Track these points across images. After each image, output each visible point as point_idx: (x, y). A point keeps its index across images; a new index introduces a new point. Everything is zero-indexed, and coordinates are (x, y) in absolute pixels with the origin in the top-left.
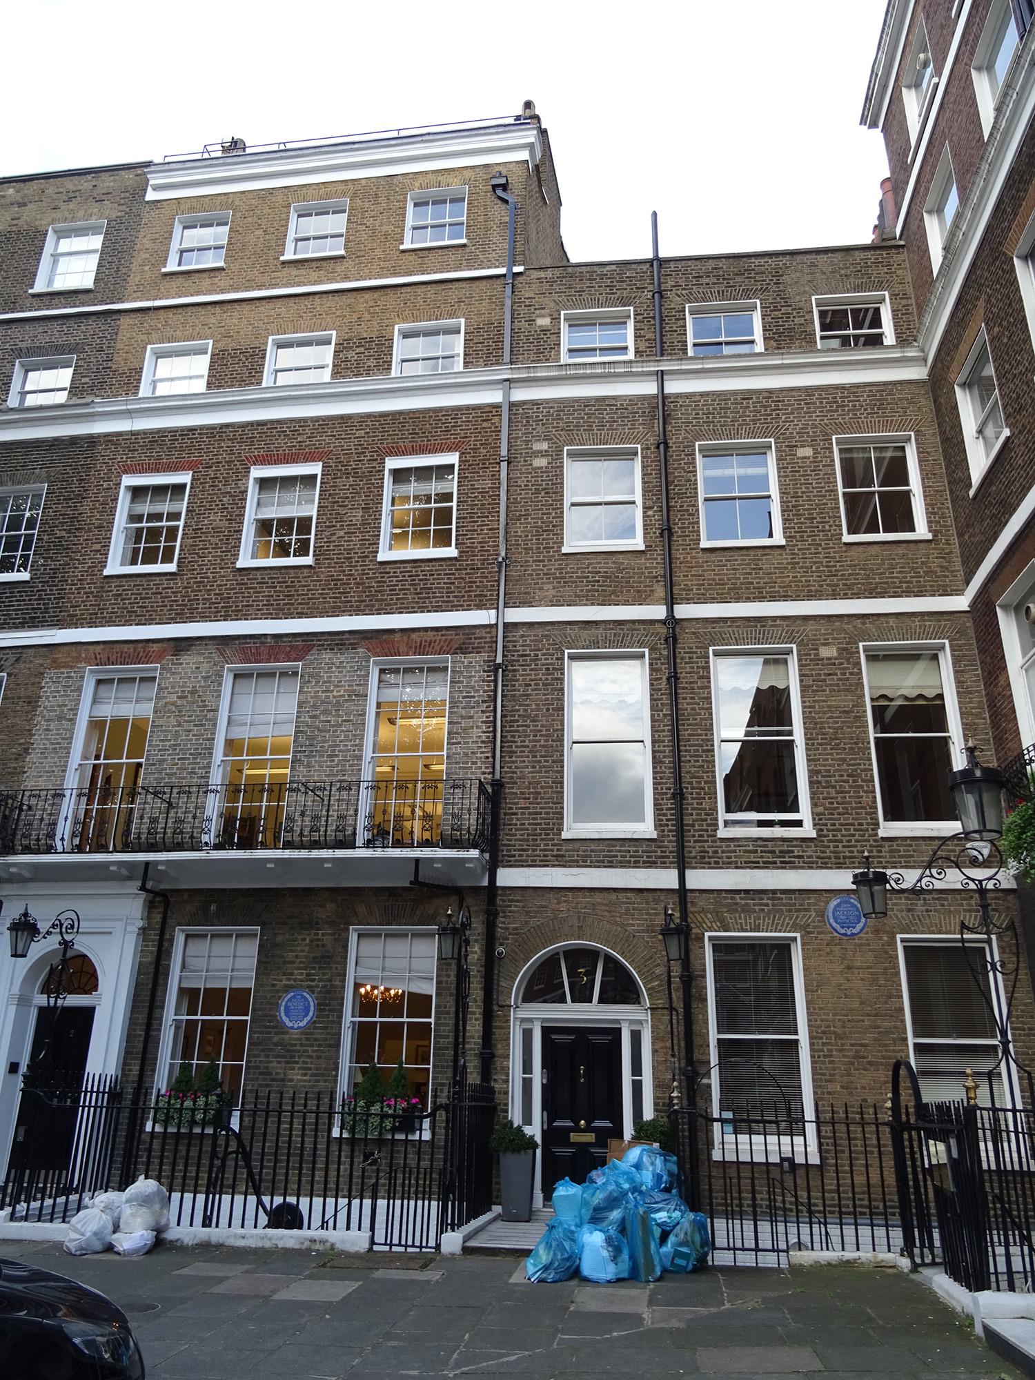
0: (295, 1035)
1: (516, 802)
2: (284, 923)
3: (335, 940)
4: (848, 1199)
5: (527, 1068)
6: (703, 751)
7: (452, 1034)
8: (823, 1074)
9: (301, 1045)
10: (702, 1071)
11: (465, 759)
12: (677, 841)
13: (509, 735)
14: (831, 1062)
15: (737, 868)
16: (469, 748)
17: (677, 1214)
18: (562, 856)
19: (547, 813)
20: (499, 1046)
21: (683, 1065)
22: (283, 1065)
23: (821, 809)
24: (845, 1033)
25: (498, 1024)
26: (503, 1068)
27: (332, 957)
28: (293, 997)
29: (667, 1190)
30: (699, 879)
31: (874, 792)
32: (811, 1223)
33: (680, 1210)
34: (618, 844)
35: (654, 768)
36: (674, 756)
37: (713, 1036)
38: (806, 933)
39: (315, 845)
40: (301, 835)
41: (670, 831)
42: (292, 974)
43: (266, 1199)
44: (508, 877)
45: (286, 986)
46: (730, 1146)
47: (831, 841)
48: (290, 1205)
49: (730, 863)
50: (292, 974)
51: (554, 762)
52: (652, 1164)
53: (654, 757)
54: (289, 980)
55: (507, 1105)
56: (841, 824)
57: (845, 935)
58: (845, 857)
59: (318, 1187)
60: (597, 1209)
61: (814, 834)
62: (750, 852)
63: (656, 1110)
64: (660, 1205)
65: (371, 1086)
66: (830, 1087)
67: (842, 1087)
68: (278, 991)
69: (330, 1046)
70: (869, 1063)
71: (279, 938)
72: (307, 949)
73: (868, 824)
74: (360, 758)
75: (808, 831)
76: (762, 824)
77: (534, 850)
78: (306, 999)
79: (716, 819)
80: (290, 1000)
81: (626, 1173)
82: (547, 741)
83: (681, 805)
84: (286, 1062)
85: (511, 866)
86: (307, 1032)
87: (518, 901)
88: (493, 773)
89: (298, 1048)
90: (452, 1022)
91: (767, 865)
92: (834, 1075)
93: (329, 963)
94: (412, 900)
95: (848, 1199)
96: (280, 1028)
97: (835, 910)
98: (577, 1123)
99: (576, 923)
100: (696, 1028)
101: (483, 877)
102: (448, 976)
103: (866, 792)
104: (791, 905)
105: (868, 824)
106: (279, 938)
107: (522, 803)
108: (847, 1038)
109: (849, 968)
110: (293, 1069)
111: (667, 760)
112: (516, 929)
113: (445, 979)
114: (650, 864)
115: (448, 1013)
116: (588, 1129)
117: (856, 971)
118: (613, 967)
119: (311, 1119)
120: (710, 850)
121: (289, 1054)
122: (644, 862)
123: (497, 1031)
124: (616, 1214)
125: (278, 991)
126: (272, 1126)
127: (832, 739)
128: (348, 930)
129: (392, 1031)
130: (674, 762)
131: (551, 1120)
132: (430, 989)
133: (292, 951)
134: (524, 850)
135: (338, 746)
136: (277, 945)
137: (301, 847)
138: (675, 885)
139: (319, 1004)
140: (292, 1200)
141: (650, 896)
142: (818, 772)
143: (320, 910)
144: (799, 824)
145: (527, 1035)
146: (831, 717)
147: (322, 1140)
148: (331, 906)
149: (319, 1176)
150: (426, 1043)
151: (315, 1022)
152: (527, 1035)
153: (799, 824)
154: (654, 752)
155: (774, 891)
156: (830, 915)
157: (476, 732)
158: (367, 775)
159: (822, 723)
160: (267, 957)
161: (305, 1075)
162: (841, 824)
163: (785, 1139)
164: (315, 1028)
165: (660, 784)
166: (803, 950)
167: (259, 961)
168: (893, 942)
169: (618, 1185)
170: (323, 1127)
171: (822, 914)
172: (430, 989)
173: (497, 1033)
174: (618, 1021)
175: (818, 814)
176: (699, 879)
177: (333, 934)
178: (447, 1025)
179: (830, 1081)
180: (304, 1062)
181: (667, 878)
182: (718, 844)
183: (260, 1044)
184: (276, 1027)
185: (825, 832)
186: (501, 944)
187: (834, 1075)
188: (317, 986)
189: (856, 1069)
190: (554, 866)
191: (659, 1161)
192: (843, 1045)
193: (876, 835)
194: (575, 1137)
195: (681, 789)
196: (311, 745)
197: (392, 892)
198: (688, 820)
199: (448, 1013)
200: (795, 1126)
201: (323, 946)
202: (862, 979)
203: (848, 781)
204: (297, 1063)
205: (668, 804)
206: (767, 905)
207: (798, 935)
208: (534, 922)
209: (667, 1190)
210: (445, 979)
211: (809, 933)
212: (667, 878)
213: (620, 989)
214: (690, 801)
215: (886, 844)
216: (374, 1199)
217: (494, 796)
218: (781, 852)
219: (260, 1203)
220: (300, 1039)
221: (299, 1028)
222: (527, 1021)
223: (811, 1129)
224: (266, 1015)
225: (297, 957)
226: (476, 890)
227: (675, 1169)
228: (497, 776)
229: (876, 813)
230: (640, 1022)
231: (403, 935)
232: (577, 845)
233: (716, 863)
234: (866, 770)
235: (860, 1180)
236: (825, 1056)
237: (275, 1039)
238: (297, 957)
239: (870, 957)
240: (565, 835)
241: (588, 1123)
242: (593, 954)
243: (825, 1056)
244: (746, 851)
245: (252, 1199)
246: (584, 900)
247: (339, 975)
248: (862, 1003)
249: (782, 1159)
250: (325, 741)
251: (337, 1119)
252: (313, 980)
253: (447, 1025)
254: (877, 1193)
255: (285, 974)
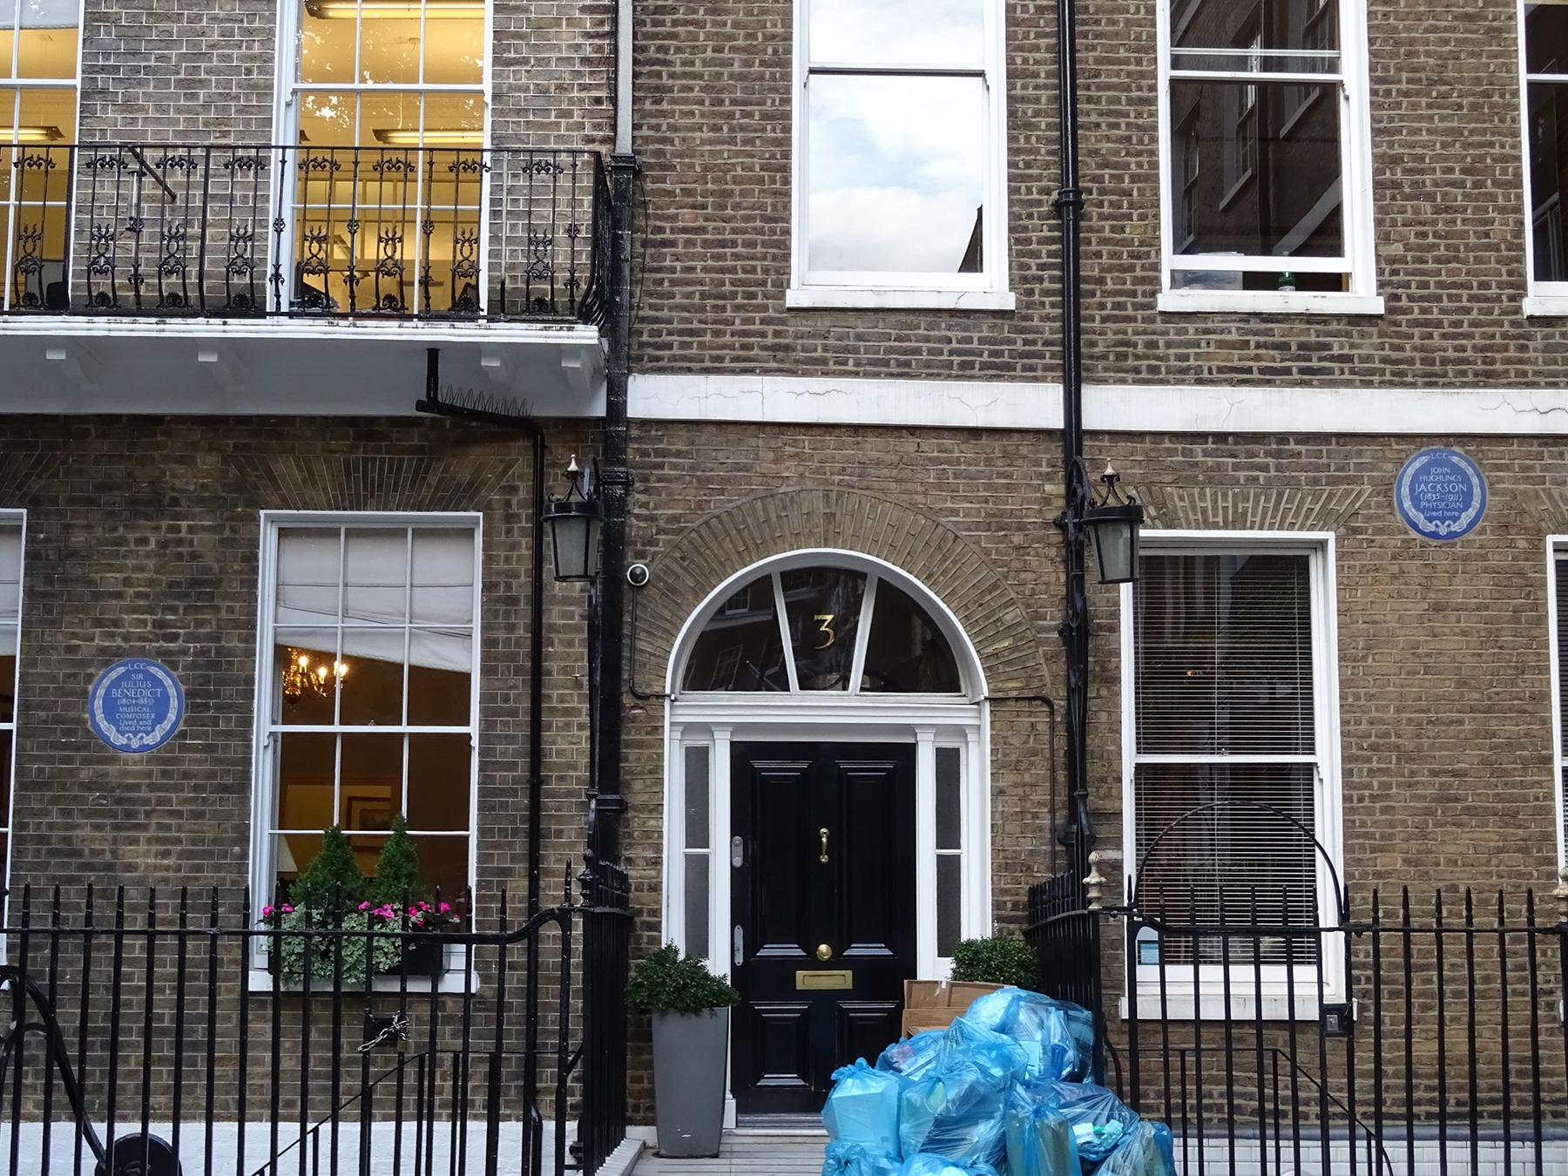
0: (135, 764)
1: (673, 210)
2: (89, 502)
3: (223, 542)
4: (1519, 1088)
5: (698, 832)
6: (1130, 101)
7: (523, 762)
8: (1367, 836)
9: (152, 787)
10: (1103, 832)
11: (540, 103)
12: (1063, 318)
13: (653, 44)
14: (1385, 810)
15: (1200, 382)
16: (550, 75)
17: (1115, 1126)
18: (787, 348)
19: (750, 244)
20: (638, 786)
21: (1059, 822)
22: (109, 833)
23: (1397, 249)
24: (1419, 748)
25: (633, 736)
26: (647, 834)
27: (217, 583)
28: (125, 677)
29: (1075, 1078)
30: (1112, 406)
31: (1519, 210)
32: (1353, 1139)
33: (1122, 1119)
34: (923, 321)
35: (1012, 139)
36: (1061, 113)
37: (1130, 758)
38: (1349, 532)
39: (173, 306)
40: (137, 279)
41: (1045, 293)
42: (116, 623)
43: (100, 1129)
44: (654, 396)
45: (103, 651)
46: (1170, 989)
47: (1416, 323)
48: (157, 1145)
49: (1185, 371)
50: (116, 623)
51: (765, 116)
52: (1041, 1025)
53: (1011, 114)
54: (112, 636)
55: (657, 913)
56: (1440, 285)
57: (1434, 535)
58: (1445, 361)
59: (226, 1098)
60: (942, 1123)
61: (1377, 306)
62: (1232, 345)
63: (997, 918)
64: (1078, 1110)
65: (324, 882)
66: (1382, 862)
67: (1406, 861)
68: (84, 663)
69: (224, 789)
70: (1467, 811)
71: (79, 539)
72: (151, 563)
73: (1500, 286)
74: (265, 90)
75: (1364, 297)
76: (1253, 281)
77: (717, 334)
78: (158, 682)
79: (1156, 267)
80: (115, 684)
81: (990, 1047)
82: (748, 63)
83: (1077, 230)
84: (116, 827)
85: (662, 371)
86: (165, 757)
87: (678, 454)
88: (612, 140)
89: (144, 794)
90: (523, 733)
91: (1270, 377)
92: (1391, 836)
93: (211, 596)
94: (423, 446)
95: (1519, 1088)
96: (96, 750)
97: (1415, 480)
98: (811, 949)
99: (819, 504)
100: (1093, 742)
101: (591, 398)
102: (511, 628)
103: (1502, 210)
104: (1318, 468)
105: (1500, 286)
106: (79, 539)
107: (687, 217)
108: (1423, 759)
109: (1438, 608)
110: (135, 841)
111: (1043, 122)
112: (675, 519)
113: (501, 635)
114: (998, 370)
115: (513, 713)
116: (837, 962)
117: (1453, 616)
118: (898, 608)
119: (196, 950)
120: (1140, 340)
121: (123, 808)
122: (984, 366)
123: (632, 753)
124: (983, 1132)
125: (84, 663)
126: (102, 971)
127: (1432, 83)
128: (256, 520)
129: (373, 759)
130: (1061, 127)
131: (751, 946)
132: (468, 659)
133: (111, 568)
134: (691, 333)
135: (206, 56)
136: (73, 554)
137: (139, 310)
138: (1057, 421)
139: (189, 694)
140: (161, 1130)
141: (996, 446)
142: (1396, 160)
143: (181, 470)
144: (1335, 282)
145: (697, 761)
146: (1435, 29)
147: (227, 993)
148: (207, 462)
149: (226, 1072)
150: (384, 791)
151: (183, 735)
152: (697, 761)
153: (1335, 282)
154: (1011, 99)
155: (1282, 437)
156: (1405, 490)
157: (566, 37)
158: (284, 131)
159: (1412, 42)
160: (49, 580)
161: (166, 854)
162: (1440, 285)
163: (1274, 974)
164: (183, 748)
165: (1023, 178)
166: (1340, 569)
167: (30, 593)
168: (1537, 552)
169: (983, 1070)
170: (228, 968)
171: (1386, 489)
172: (468, 659)
173: (632, 758)
174: (910, 729)
175: (1391, 260)
176: (1112, 406)
177: (219, 529)
178: (512, 739)
179: (1381, 849)
180: (160, 827)
181: (1036, 404)
182: (1159, 325)
183: (47, 785)
184: (85, 747)
185: (1404, 302)
186: (640, 555)
187: (1391, 836)
188: (185, 652)
189: (1437, 824)
190: (766, 372)
191: (1055, 1019)
192: (1413, 773)
193: (1518, 310)
194: (805, 980)
195: (1078, 192)
196: (134, 54)
197: (364, 429)
198: (1090, 268)
199: (513, 713)
200: (1298, 943)
201: (194, 556)
202: (1464, 633)
203: (1462, 185)
204: (145, 827)
205: (1042, 228)
206: (1266, 468)
207: (1330, 536)
208: (718, 504)
209: (1075, 1078)
210: (501, 635)
211: (1356, 531)
212: (1036, 404)
213: (914, 655)
214: (1095, 223)
215: (1539, 332)
216: (366, 1122)
217: (618, 190)
218: (1301, 346)
219: (83, 1131)
220: (149, 774)
221: (144, 748)
222: (701, 730)
223: (1333, 946)
224: (58, 720)
225: (126, 582)
226: (575, 428)
227: (1088, 1035)
228: (625, 146)
229: (1520, 260)
230: (960, 731)
231: (394, 533)
232: (824, 323)
233: (1153, 370)
234: (1504, 159)
235: (1425, 1049)
236: (1373, 798)
237: (86, 774)
238: (126, 582)
239: (1485, 583)
240: (794, 298)
241: (837, 950)
242: (850, 579)
243: (1373, 798)
244: (1222, 344)
245: (64, 1131)
246: (837, 451)
247: (237, 624)
248: (1461, 683)
249: (1325, 1009)
250: (170, 44)
251: (260, 946)
252: (174, 638)
253: (512, 739)
254: (1457, 1077)
255: (98, 623)
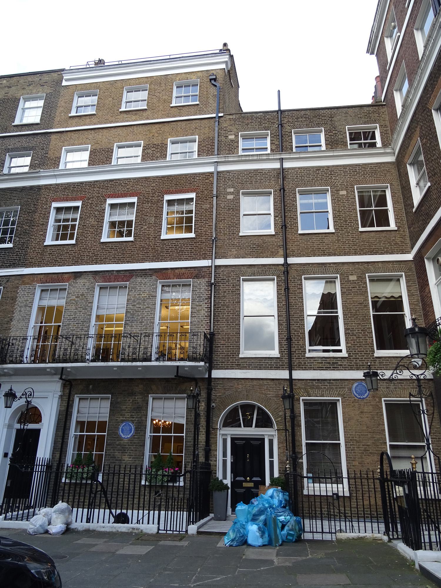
0: (126, 441)
1: (220, 342)
2: (121, 393)
3: (143, 401)
4: (361, 511)
5: (225, 455)
6: (300, 320)
7: (192, 441)
8: (350, 458)
9: (128, 445)
10: (299, 456)
11: (198, 324)
12: (288, 358)
13: (217, 313)
14: (354, 453)
15: (314, 370)
16: (200, 319)
17: (288, 517)
18: (240, 365)
19: (233, 347)
20: (213, 446)
21: (291, 454)
22: (121, 454)
23: (350, 345)
24: (360, 440)
25: (212, 436)
26: (214, 455)
27: (141, 408)
28: (125, 425)
29: (284, 507)
30: (298, 374)
31: (372, 337)
32: (345, 521)
33: (290, 516)
34: (263, 359)
35: (279, 327)
36: (287, 322)
37: (304, 441)
38: (343, 398)
39: (134, 360)
40: (128, 356)
41: (285, 354)
42: (124, 415)
43: (113, 511)
44: (216, 374)
45: (122, 420)
46: (311, 488)
47: (354, 358)
48: (124, 513)
49: (311, 368)
50: (124, 415)
51: (236, 324)
52: (278, 496)
53: (279, 323)
54: (123, 417)
55: (216, 471)
56: (358, 351)
57: (360, 398)
58: (360, 365)
59: (136, 506)
60: (254, 515)
61: (347, 355)
62: (320, 363)
63: (279, 473)
64: (281, 514)
65: (158, 463)
66: (354, 463)
67: (359, 463)
68: (118, 422)
69: (141, 446)
70: (370, 453)
71: (119, 400)
72: (131, 404)
73: (370, 351)
74: (153, 323)
75: (344, 354)
76: (324, 351)
77: (227, 362)
78: (130, 426)
79: (305, 349)
80: (123, 426)
81: (267, 500)
82: (233, 316)
83: (290, 343)
84: (122, 453)
85: (218, 369)
86: (131, 440)
87: (221, 384)
88: (210, 329)
89: (127, 446)
90: (193, 435)
91: (327, 369)
92: (355, 458)
93: (140, 410)
94: (176, 383)
95: (361, 511)
96: (119, 438)
97: (356, 388)
98: (246, 478)
99: (245, 393)
100: (297, 438)
101: (206, 374)
102: (191, 416)
103: (369, 337)
104: (337, 386)
105: (370, 351)
106: (119, 400)
107: (222, 342)
108: (361, 442)
109: (362, 412)
110: (125, 455)
111: (284, 324)
112: (220, 396)
113: (189, 417)
114: (277, 368)
115: (191, 432)
116: (251, 481)
117: (365, 414)
118: (261, 412)
119: (132, 477)
120: (303, 362)
121: (123, 449)
122: (275, 367)
123: (212, 439)
124: (262, 517)
125: (118, 422)
126: (116, 480)
127: (354, 315)
128: (148, 396)
129: (167, 439)
130: (287, 325)
131: (235, 477)
132: (183, 421)
133: (124, 405)
134: (223, 362)
135: (144, 318)
136: (118, 403)
137: (128, 361)
138: (288, 377)
139: (136, 428)
140: (124, 511)
141: (277, 382)
142: (349, 329)
143: (136, 388)
144: (340, 351)
145: (225, 441)
146: (354, 306)
147: (137, 486)
148: (141, 386)
149: (136, 501)
150: (181, 444)
151: (134, 436)
152: (225, 441)
153: (340, 351)
154: (278, 320)
155: (330, 380)
156: (354, 390)
157: (203, 312)
158: (156, 330)
159: (350, 308)
160: (114, 408)
161: (130, 458)
162: (358, 351)
163: (335, 486)
164: (134, 438)
165: (281, 334)
166: (342, 405)
167: (110, 409)
168: (380, 401)
169: (263, 505)
170: (138, 480)
171: (350, 389)
172: (183, 421)
173: (212, 440)
174: (263, 435)
175: (349, 347)
176: (298, 374)
177: (142, 398)
178: (191, 437)
179: (354, 461)
180: (130, 453)
181: (284, 374)
182: (306, 359)
183: (111, 445)
184: (118, 438)
185: (352, 355)
186: (214, 402)
187: (355, 458)
188: (135, 420)
189: (365, 456)
190: (236, 369)
191: (281, 495)
192: (359, 445)
193: (373, 356)
194: (245, 485)
195: (290, 336)
196: (133, 318)
197: (167, 380)
198: (293, 350)
199: (191, 432)
200: (339, 480)
201: (138, 403)
202: (367, 417)
203: (361, 333)
204: (127, 453)
205: (285, 343)
206: (327, 386)
207: (340, 398)
208: (227, 393)
209: (284, 507)
210: (189, 417)
211: (345, 397)
212: (284, 374)
213: (264, 421)
214: (294, 341)
215: (378, 360)
216: (160, 511)
217: (211, 339)
218: (333, 363)
219: (111, 512)
220: (128, 443)
221: (127, 438)
222: (225, 435)
223: (345, 481)
224: (113, 433)
225: (126, 408)
226: (203, 379)
227: (287, 498)
228: (212, 331)
229: (373, 346)
230: (273, 436)
231: (172, 398)
232: (246, 360)
233: (305, 368)
234: (369, 328)
235: (366, 503)
236: (351, 450)
237: (117, 443)
238: (126, 408)
239: (371, 408)
240: (241, 356)
241: (251, 478)
242: (253, 407)
243: (351, 450)
244: (318, 363)
245: (107, 511)
246: (249, 383)
247: (144, 415)
248: (367, 427)
249: (333, 494)
250: (139, 316)
251: (144, 477)
252: (133, 418)
253: (191, 437)
254: (373, 508)
255: (121, 415)
